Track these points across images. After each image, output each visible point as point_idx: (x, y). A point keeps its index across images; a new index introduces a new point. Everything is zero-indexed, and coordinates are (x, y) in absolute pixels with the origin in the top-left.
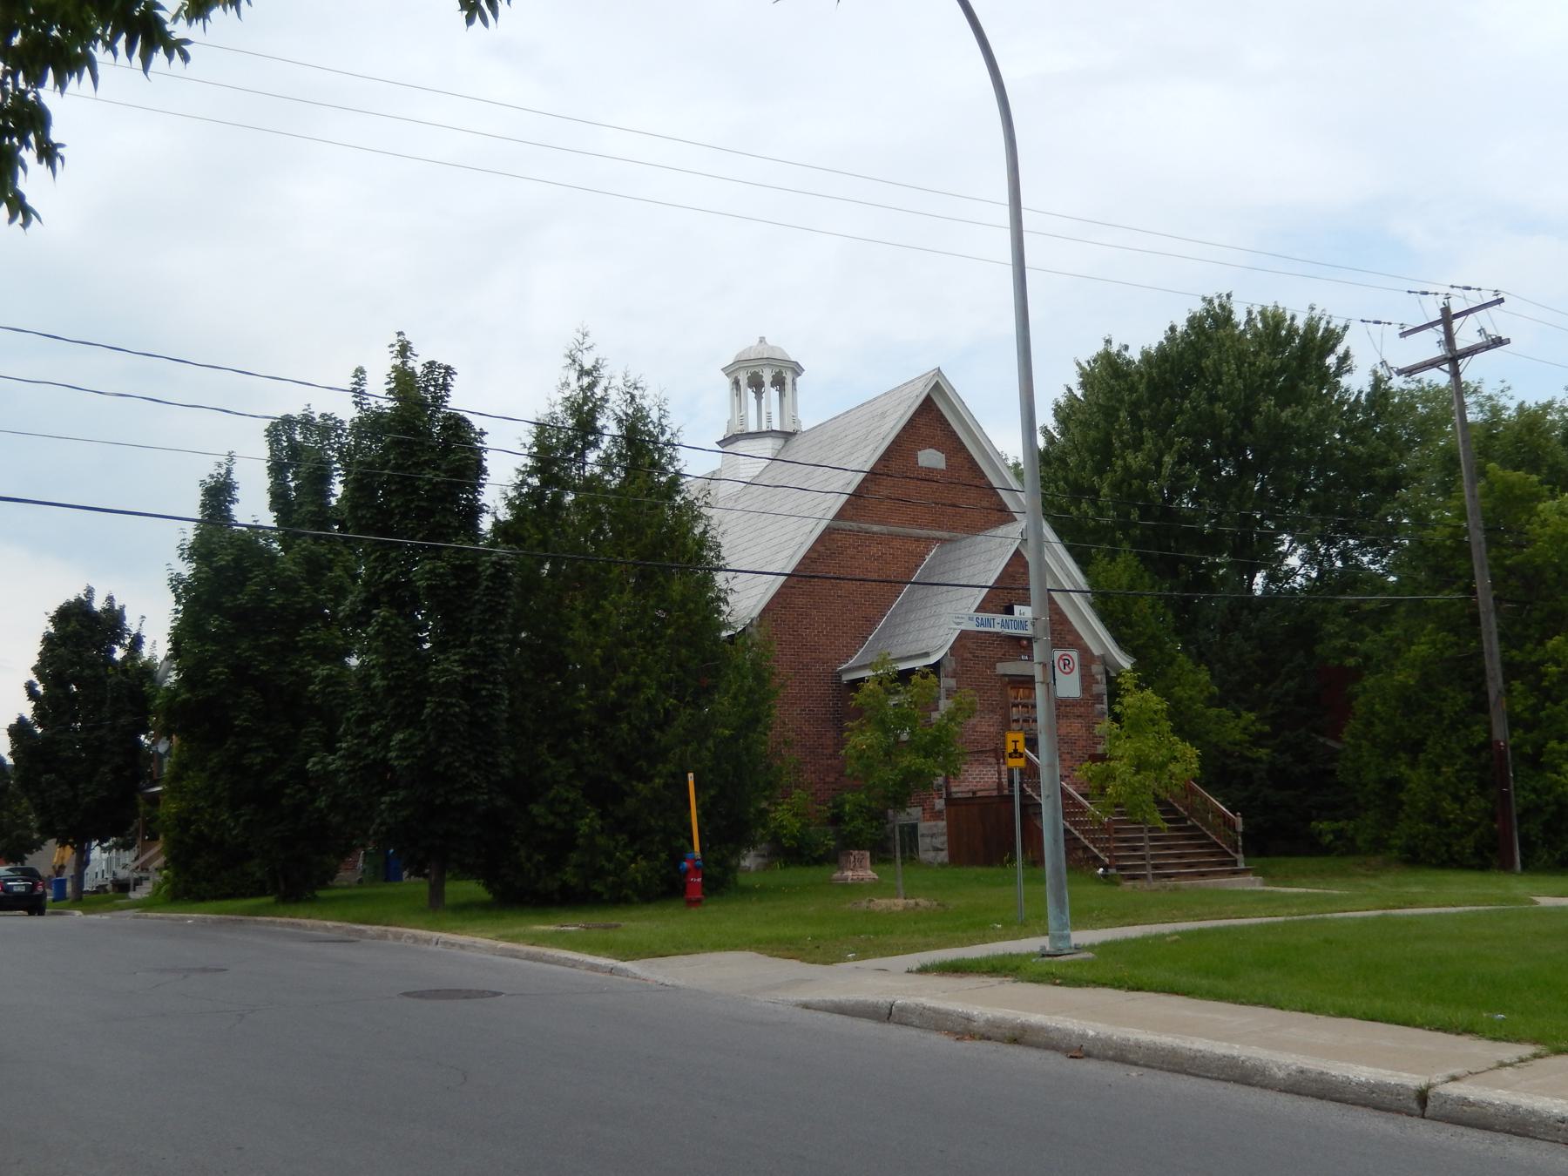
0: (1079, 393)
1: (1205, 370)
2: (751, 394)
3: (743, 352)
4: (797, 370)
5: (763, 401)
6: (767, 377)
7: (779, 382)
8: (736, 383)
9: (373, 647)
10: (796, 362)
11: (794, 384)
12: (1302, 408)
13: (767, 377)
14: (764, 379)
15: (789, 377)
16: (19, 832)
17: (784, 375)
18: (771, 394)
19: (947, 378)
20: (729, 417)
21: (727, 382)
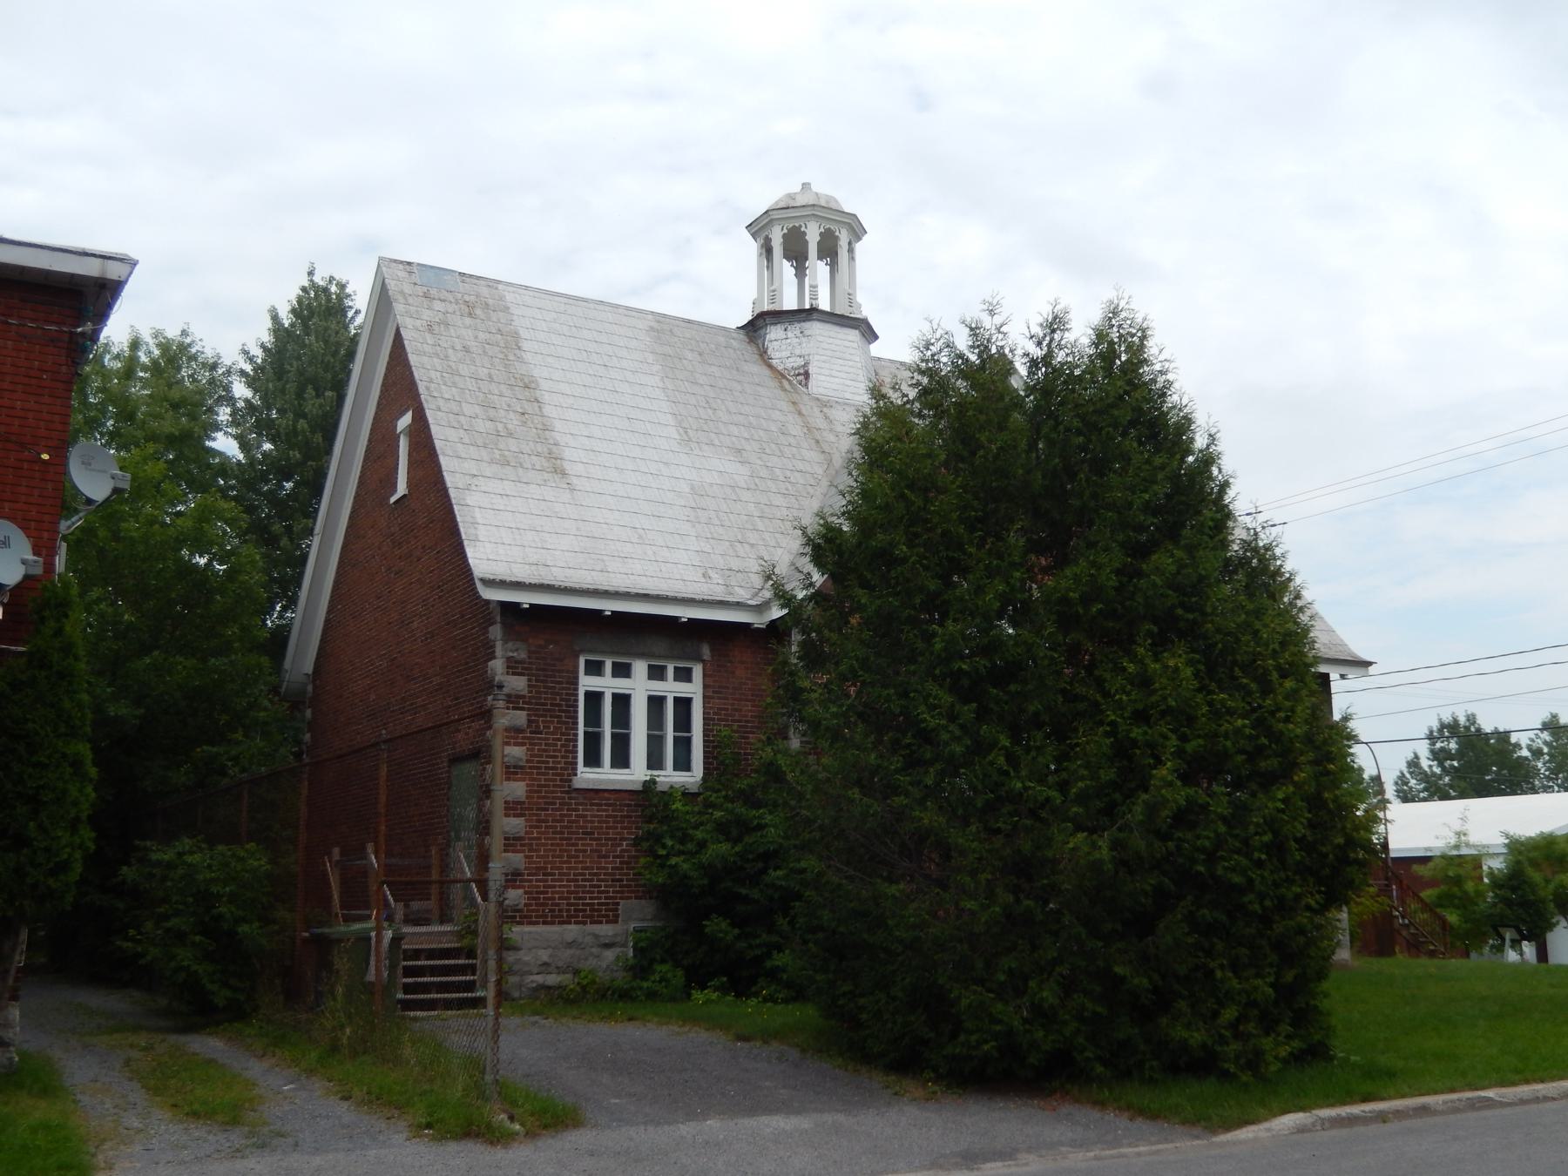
0: (818, 578)
1: (341, 963)
2: (788, 269)
3: (780, 200)
4: (857, 231)
5: (807, 279)
6: (813, 235)
7: (828, 250)
8: (767, 250)
9: (1259, 742)
10: (855, 215)
11: (851, 250)
12: (224, 390)
13: (813, 235)
14: (772, 244)
15: (844, 237)
16: (1223, 853)
17: (837, 233)
18: (819, 270)
19: (449, 268)
20: (755, 295)
21: (752, 247)
